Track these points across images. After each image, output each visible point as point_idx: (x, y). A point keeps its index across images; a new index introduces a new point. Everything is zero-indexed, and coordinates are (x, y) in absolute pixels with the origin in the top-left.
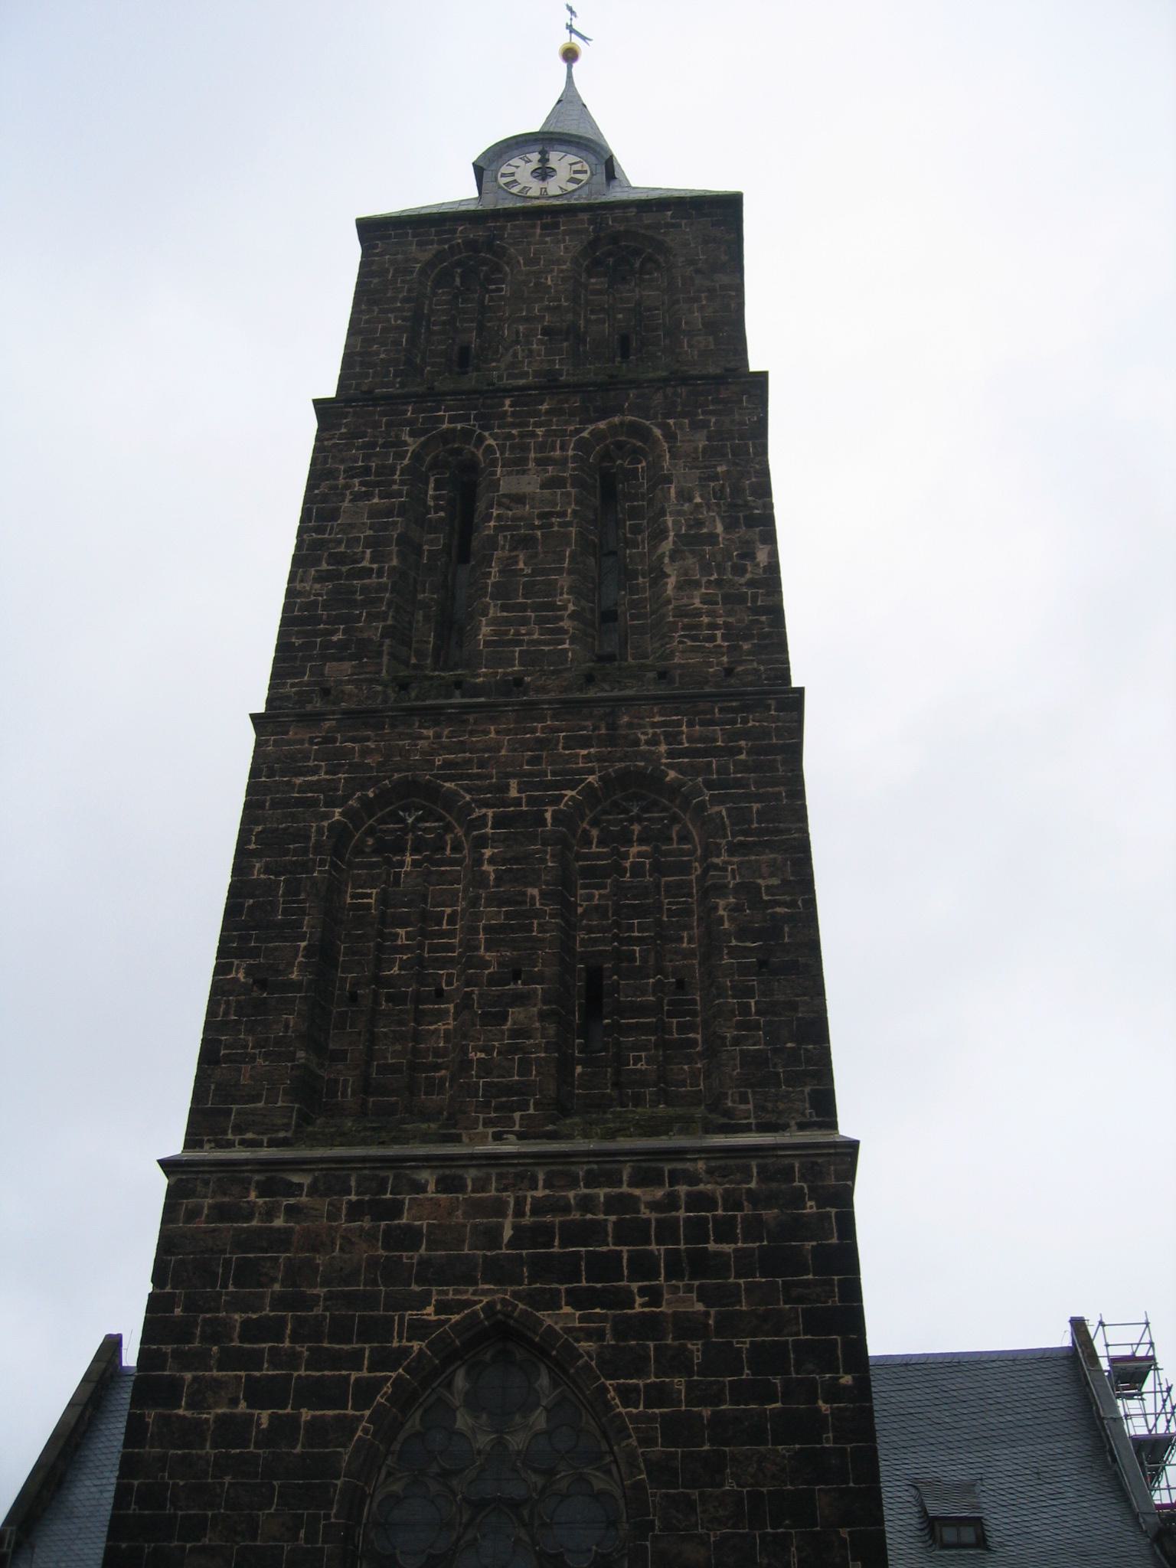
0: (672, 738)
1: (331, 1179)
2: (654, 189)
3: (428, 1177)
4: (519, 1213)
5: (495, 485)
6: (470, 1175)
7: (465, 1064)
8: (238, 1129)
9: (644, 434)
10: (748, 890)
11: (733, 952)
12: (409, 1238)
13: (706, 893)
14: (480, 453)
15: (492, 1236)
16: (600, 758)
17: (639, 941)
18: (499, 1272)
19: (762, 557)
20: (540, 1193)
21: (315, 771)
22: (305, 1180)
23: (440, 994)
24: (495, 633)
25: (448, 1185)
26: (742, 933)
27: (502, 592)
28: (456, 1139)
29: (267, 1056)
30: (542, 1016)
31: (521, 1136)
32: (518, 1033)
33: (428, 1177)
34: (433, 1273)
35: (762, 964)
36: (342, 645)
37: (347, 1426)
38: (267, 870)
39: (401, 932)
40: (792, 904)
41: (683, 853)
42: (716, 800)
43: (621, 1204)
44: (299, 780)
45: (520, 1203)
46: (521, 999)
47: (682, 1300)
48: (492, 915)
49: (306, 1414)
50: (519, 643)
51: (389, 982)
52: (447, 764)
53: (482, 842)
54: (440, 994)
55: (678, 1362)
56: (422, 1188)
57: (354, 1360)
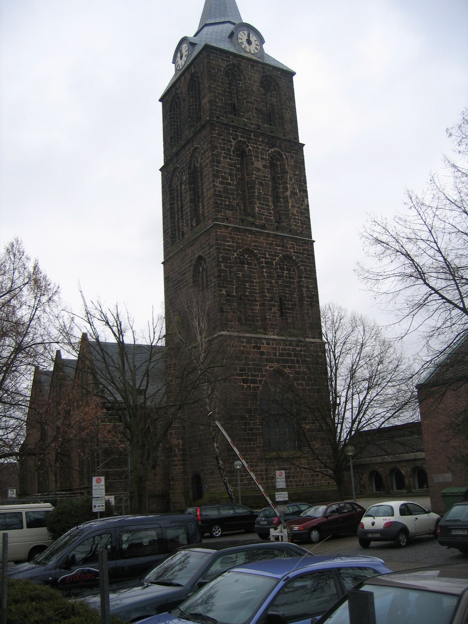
0: (293, 248)
1: (249, 341)
2: (274, 60)
3: (264, 341)
4: (279, 350)
5: (252, 163)
6: (271, 342)
7: (265, 319)
8: (231, 328)
9: (281, 155)
10: (307, 287)
11: (307, 301)
12: (262, 353)
13: (300, 287)
14: (247, 149)
15: (275, 354)
16: (282, 250)
17: (288, 294)
18: (278, 361)
19: (306, 202)
20: (282, 347)
21: (229, 242)
22: (245, 340)
23: (256, 301)
24: (259, 211)
25: (268, 344)
26: (308, 297)
27: (259, 199)
28: (266, 334)
29: (233, 312)
30: (278, 310)
31: (277, 335)
32: (274, 313)
33: (264, 341)
34: (269, 360)
35: (311, 304)
36: (229, 206)
37: (259, 387)
38: (224, 267)
39: (247, 284)
40: (314, 292)
41: (293, 274)
42: (302, 265)
43: (294, 350)
44: (227, 244)
45: (279, 348)
46: (274, 306)
47: (303, 369)
48: (267, 286)
49: (252, 385)
50: (263, 215)
51: (246, 296)
52: (254, 246)
53: (263, 267)
54: (256, 301)
55: (303, 379)
56: (263, 344)
57: (258, 376)
